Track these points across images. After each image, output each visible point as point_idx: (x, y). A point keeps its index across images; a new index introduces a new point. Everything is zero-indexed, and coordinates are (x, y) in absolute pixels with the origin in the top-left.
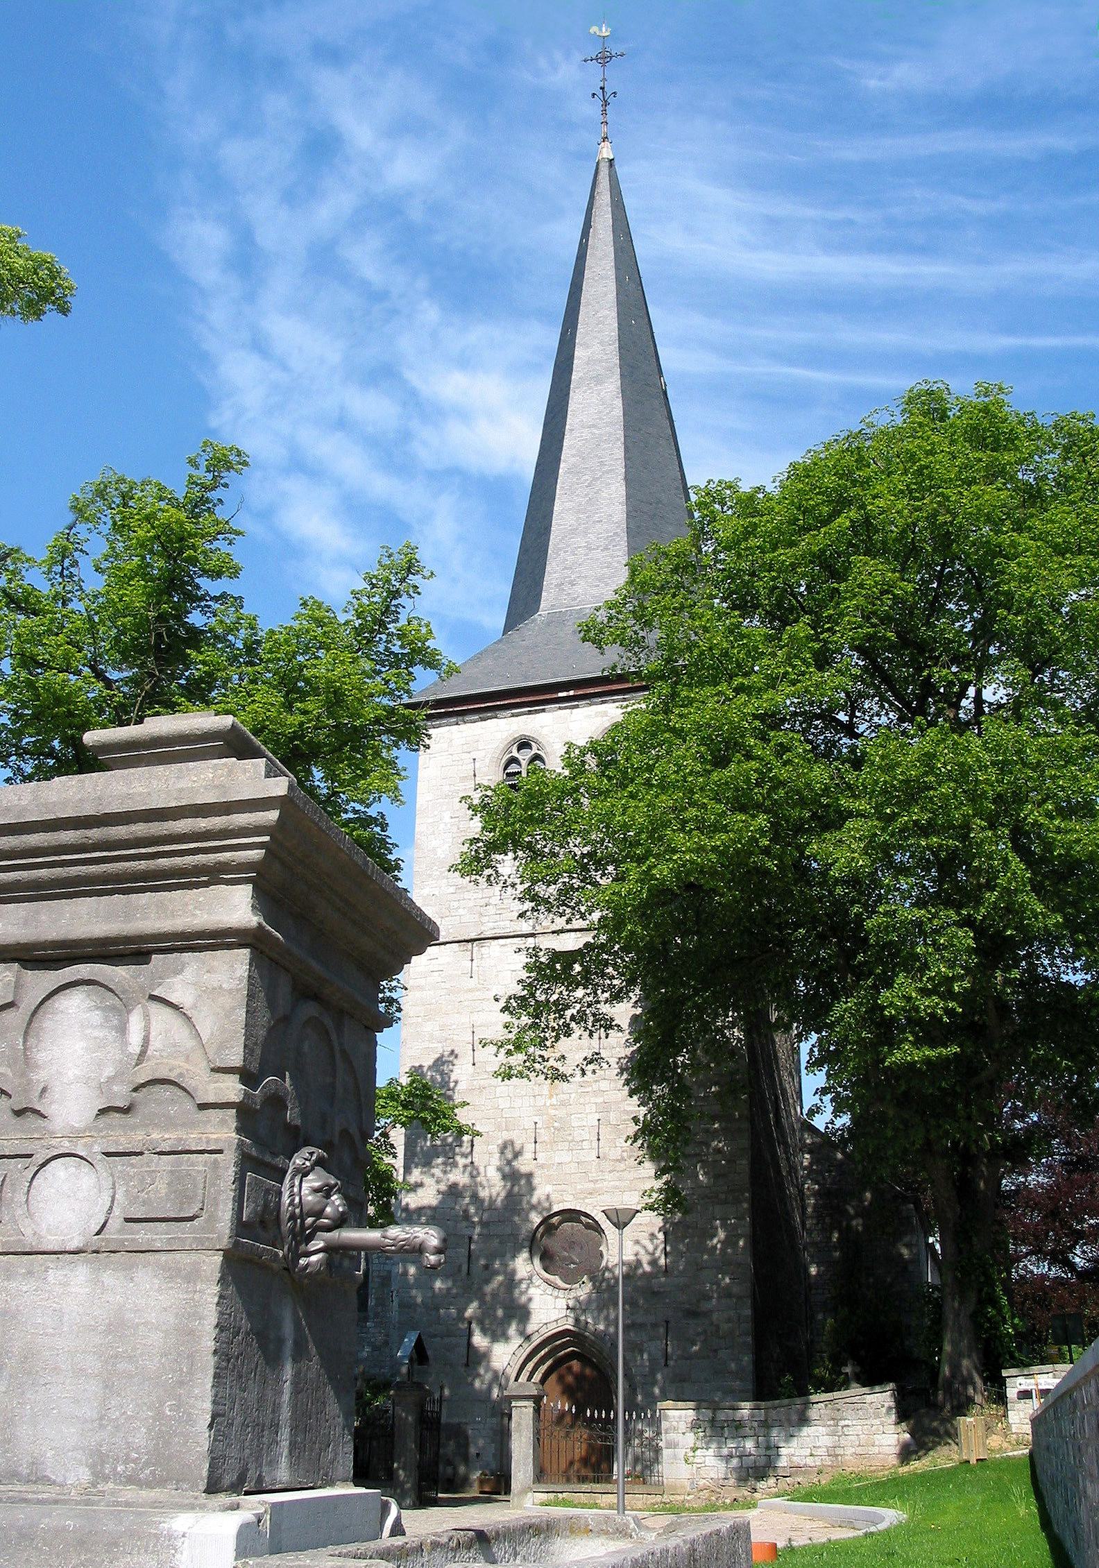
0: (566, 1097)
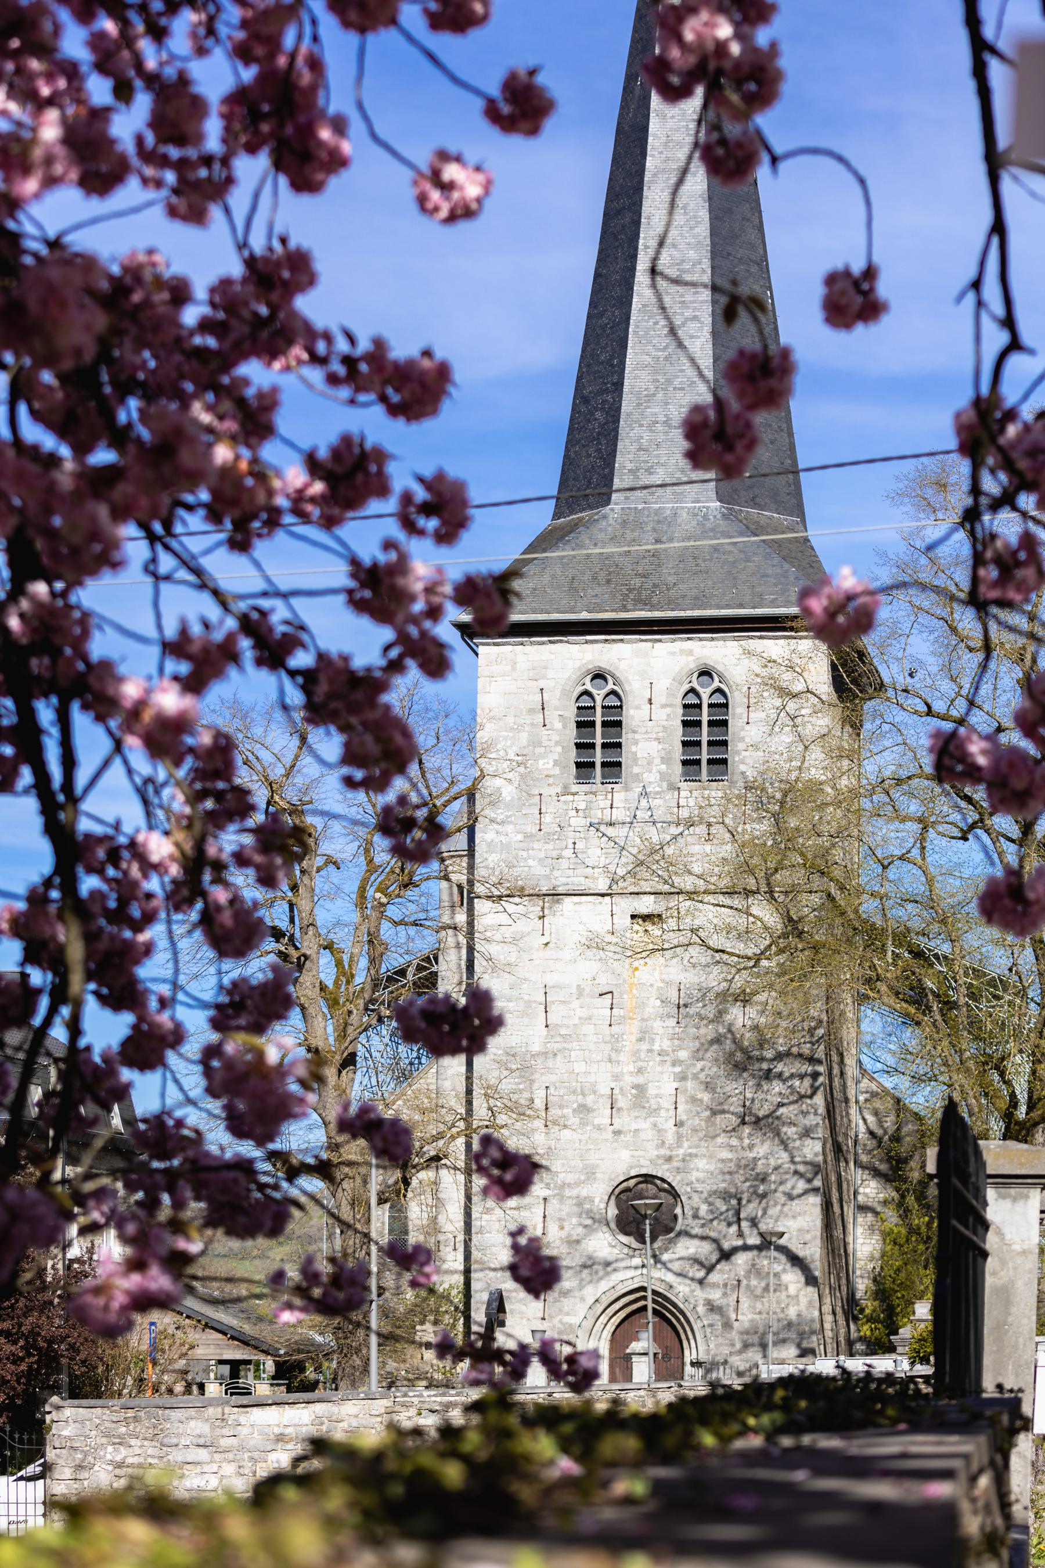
0: (644, 1064)
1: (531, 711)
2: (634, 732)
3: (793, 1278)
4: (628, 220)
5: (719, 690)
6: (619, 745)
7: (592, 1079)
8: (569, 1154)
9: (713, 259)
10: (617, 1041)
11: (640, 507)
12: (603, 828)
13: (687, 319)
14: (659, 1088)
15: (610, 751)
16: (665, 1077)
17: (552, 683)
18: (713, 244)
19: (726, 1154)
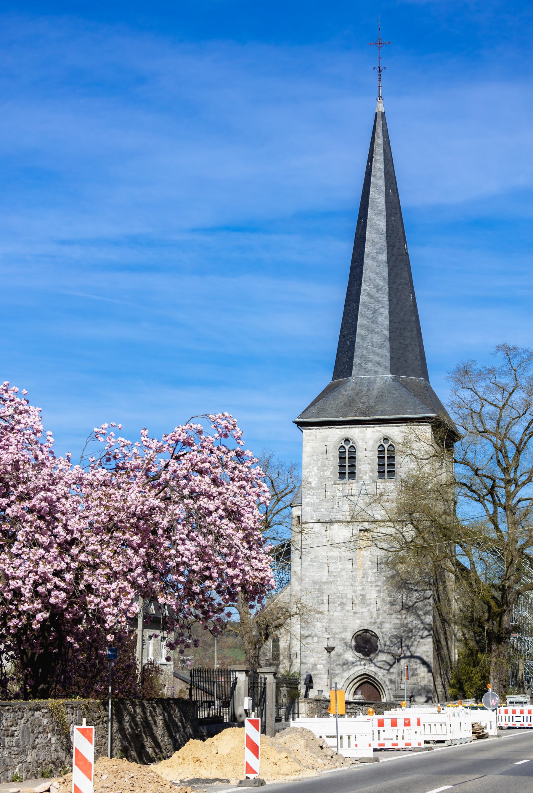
0: (365, 587)
1: (322, 454)
2: (360, 461)
3: (422, 671)
4: (358, 271)
5: (391, 445)
6: (355, 466)
7: (345, 592)
8: (337, 621)
9: (389, 285)
10: (354, 577)
11: (362, 377)
12: (349, 497)
13: (380, 307)
14: (370, 596)
15: (351, 468)
16: (373, 591)
17: (330, 443)
18: (389, 279)
19: (397, 621)
